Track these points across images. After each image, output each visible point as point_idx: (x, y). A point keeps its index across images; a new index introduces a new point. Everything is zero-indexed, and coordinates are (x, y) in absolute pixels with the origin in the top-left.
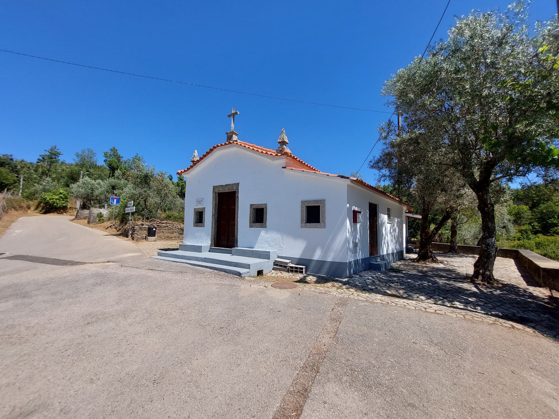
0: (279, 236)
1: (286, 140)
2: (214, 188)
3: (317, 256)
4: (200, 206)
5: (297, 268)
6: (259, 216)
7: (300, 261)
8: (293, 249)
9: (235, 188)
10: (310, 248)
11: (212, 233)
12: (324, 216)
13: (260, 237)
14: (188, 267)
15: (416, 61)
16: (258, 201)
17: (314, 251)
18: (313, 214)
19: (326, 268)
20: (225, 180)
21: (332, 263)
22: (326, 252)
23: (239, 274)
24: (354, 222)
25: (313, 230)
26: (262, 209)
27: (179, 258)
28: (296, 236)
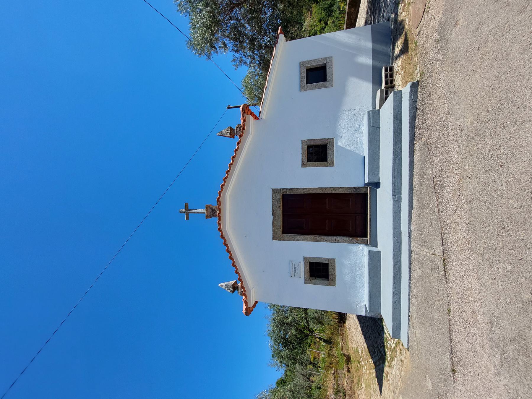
1: (232, 283)
3: (367, 60)
4: (302, 270)
5: (386, 77)
6: (318, 153)
7: (376, 81)
8: (360, 92)
9: (279, 196)
10: (357, 71)
11: (344, 241)
12: (319, 60)
13: (348, 148)
14: (422, 175)
16: (298, 154)
17: (362, 66)
20: (265, 215)
21: (373, 41)
22: (359, 50)
23: (415, 86)
25: (335, 72)
27: (401, 102)
28: (343, 92)
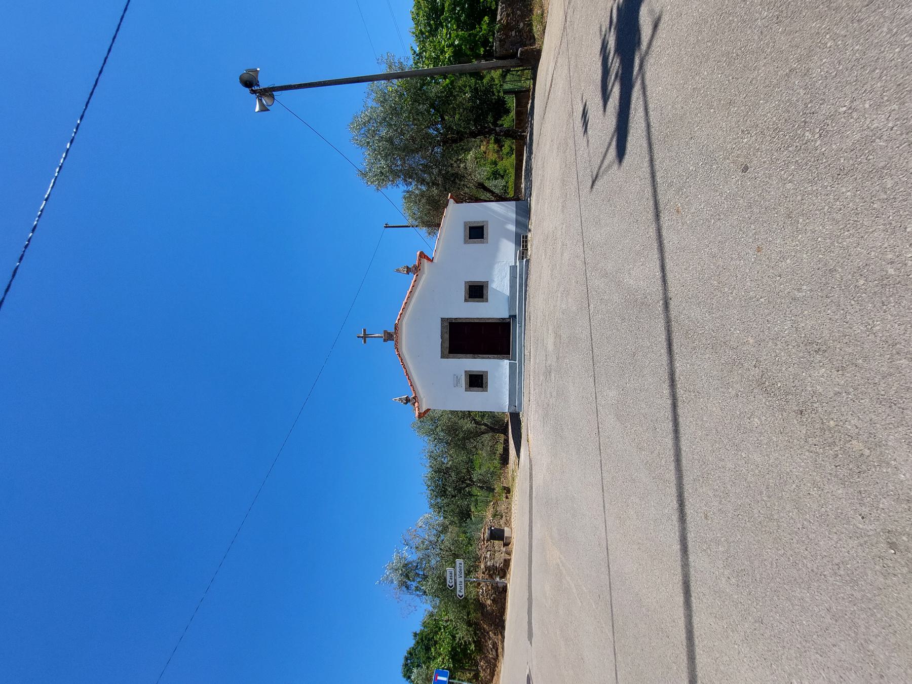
0: (496, 266)
2: (443, 356)
3: (512, 228)
4: (463, 381)
6: (477, 292)
7: (517, 243)
9: (447, 324)
12: (478, 222)
15: (362, 158)
17: (508, 230)
18: (476, 232)
19: (520, 218)
20: (435, 338)
22: (508, 220)
24: (518, 414)
25: (490, 232)
26: (471, 228)
28: (496, 249)
